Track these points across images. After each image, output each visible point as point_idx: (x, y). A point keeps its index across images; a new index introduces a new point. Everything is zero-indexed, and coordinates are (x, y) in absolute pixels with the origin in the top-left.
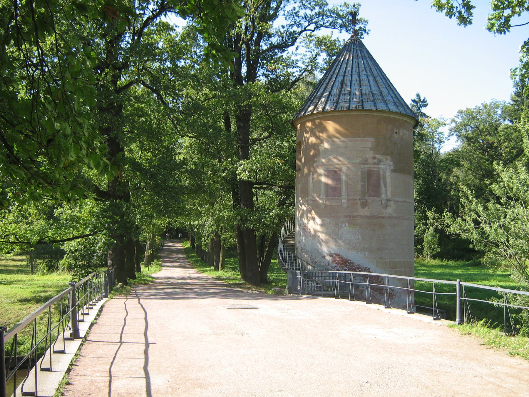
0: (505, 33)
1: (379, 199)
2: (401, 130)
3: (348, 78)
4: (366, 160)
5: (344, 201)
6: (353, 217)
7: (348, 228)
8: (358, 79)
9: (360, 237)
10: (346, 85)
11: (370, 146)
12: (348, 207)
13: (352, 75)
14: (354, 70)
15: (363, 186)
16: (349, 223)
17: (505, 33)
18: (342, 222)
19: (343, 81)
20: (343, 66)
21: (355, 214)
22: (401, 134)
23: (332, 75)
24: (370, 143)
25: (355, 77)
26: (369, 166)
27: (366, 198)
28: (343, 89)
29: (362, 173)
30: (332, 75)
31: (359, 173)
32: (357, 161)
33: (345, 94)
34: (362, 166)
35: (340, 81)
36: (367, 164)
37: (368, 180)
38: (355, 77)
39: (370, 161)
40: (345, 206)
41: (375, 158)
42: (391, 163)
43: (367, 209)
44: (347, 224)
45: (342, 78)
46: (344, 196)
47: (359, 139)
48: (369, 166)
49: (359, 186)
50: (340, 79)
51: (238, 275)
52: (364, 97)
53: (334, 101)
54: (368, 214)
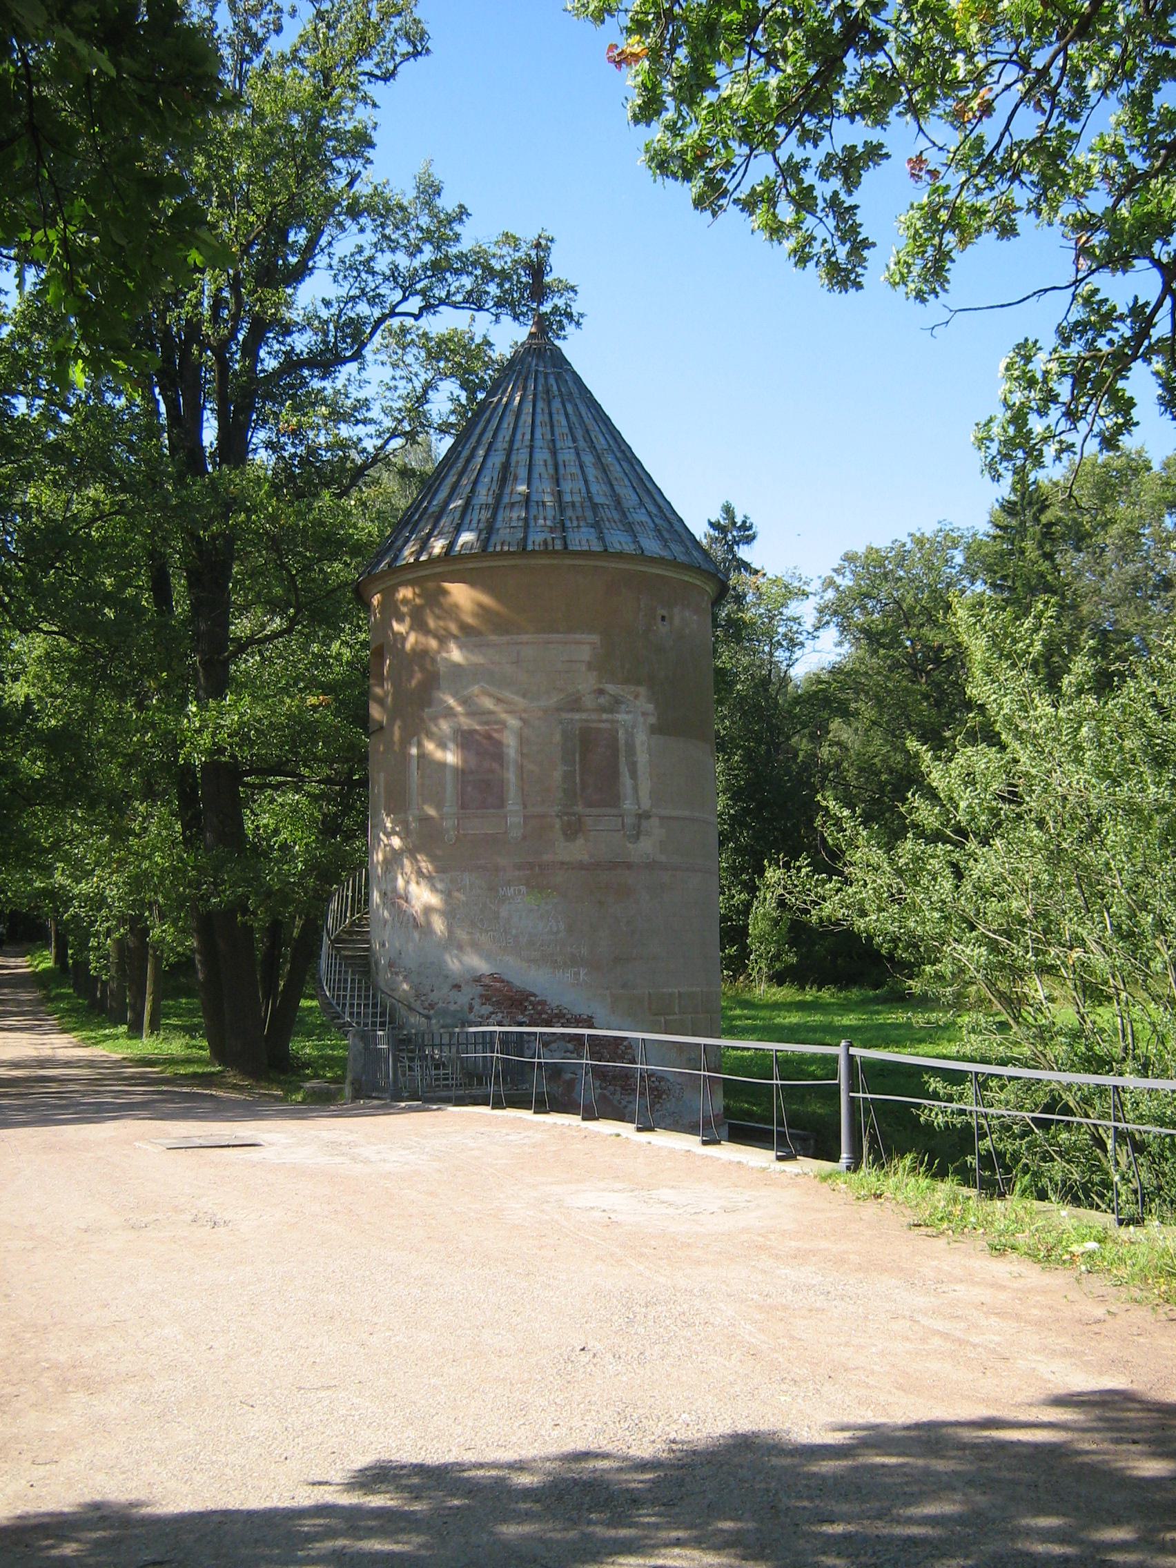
1: (614, 811)
2: (676, 610)
4: (577, 700)
9: (562, 927)
12: (524, 838)
13: (532, 447)
15: (568, 776)
16: (528, 885)
18: (509, 883)
22: (677, 621)
24: (587, 648)
25: (542, 456)
26: (584, 716)
27: (579, 809)
31: (557, 738)
34: (565, 715)
35: (498, 465)
39: (588, 701)
40: (516, 833)
41: (601, 692)
42: (650, 707)
43: (580, 841)
44: (523, 889)
45: (503, 459)
46: (513, 803)
48: (584, 716)
49: (557, 775)
53: (481, 526)
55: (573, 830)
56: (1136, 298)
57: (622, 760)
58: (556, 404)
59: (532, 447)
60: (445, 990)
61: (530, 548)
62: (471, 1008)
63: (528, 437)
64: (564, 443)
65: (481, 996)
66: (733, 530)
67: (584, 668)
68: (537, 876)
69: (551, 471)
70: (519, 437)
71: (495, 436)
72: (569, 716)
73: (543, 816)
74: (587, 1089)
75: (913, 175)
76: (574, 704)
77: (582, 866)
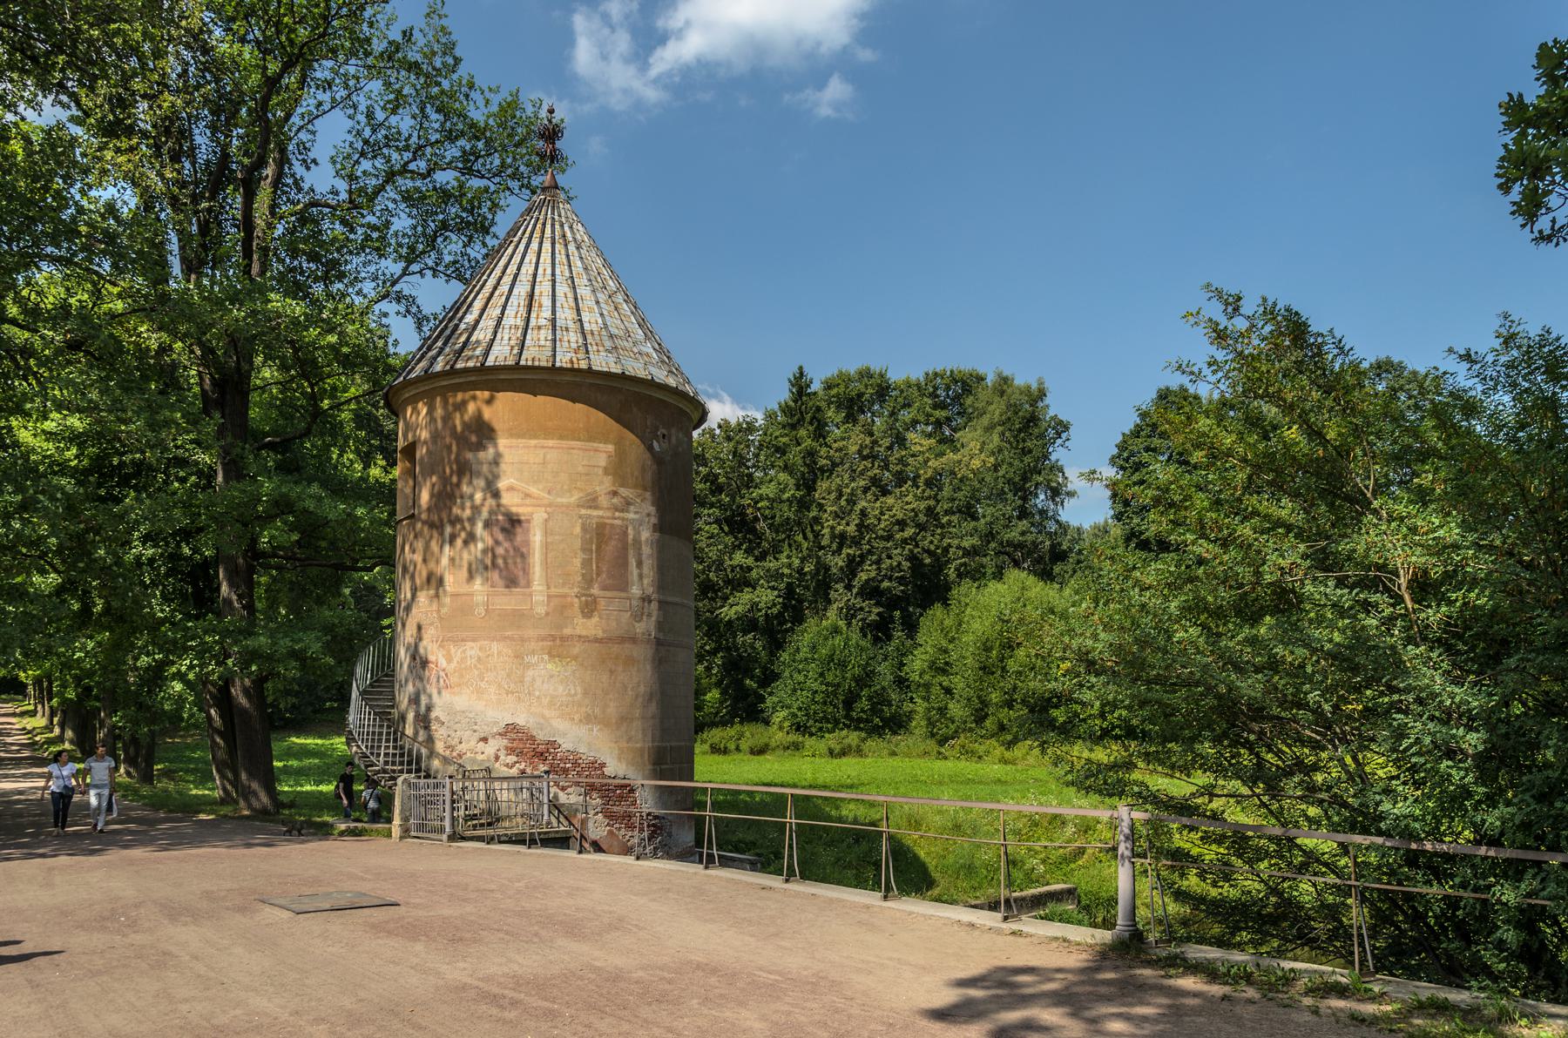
0: (1497, 175)
1: (623, 595)
2: (673, 431)
3: (543, 288)
4: (595, 499)
5: (537, 598)
6: (562, 639)
7: (549, 666)
8: (570, 295)
9: (579, 689)
10: (540, 306)
11: (603, 464)
12: (547, 614)
13: (554, 281)
14: (558, 272)
15: (586, 563)
16: (549, 654)
17: (1497, 175)
18: (533, 653)
19: (531, 296)
20: (527, 260)
21: (567, 631)
22: (674, 440)
23: (500, 278)
24: (604, 456)
25: (563, 289)
26: (601, 513)
27: (595, 591)
28: (533, 315)
29: (584, 529)
30: (500, 278)
31: (578, 530)
32: (574, 498)
33: (539, 328)
34: (583, 512)
35: (523, 294)
36: (596, 508)
37: (599, 548)
38: (563, 289)
39: (604, 501)
40: (541, 610)
41: (615, 493)
42: (652, 510)
43: (595, 620)
44: (546, 657)
45: (528, 288)
46: (538, 585)
47: (533, 442)
48: (601, 513)
49: (577, 562)
50: (522, 289)
51: (33, 714)
52: (589, 337)
53: (513, 342)
54: (600, 634)
55: (589, 609)
56: (1265, 300)
57: (631, 552)
58: (572, 247)
59: (554, 281)
60: (473, 743)
61: (523, 363)
62: (497, 758)
63: (549, 271)
64: (582, 281)
65: (507, 748)
66: (1062, 427)
67: (600, 471)
68: (558, 646)
69: (573, 304)
70: (540, 271)
71: (519, 269)
72: (589, 512)
73: (565, 596)
74: (791, 853)
75: (1543, 238)
76: (592, 502)
77: (597, 640)
